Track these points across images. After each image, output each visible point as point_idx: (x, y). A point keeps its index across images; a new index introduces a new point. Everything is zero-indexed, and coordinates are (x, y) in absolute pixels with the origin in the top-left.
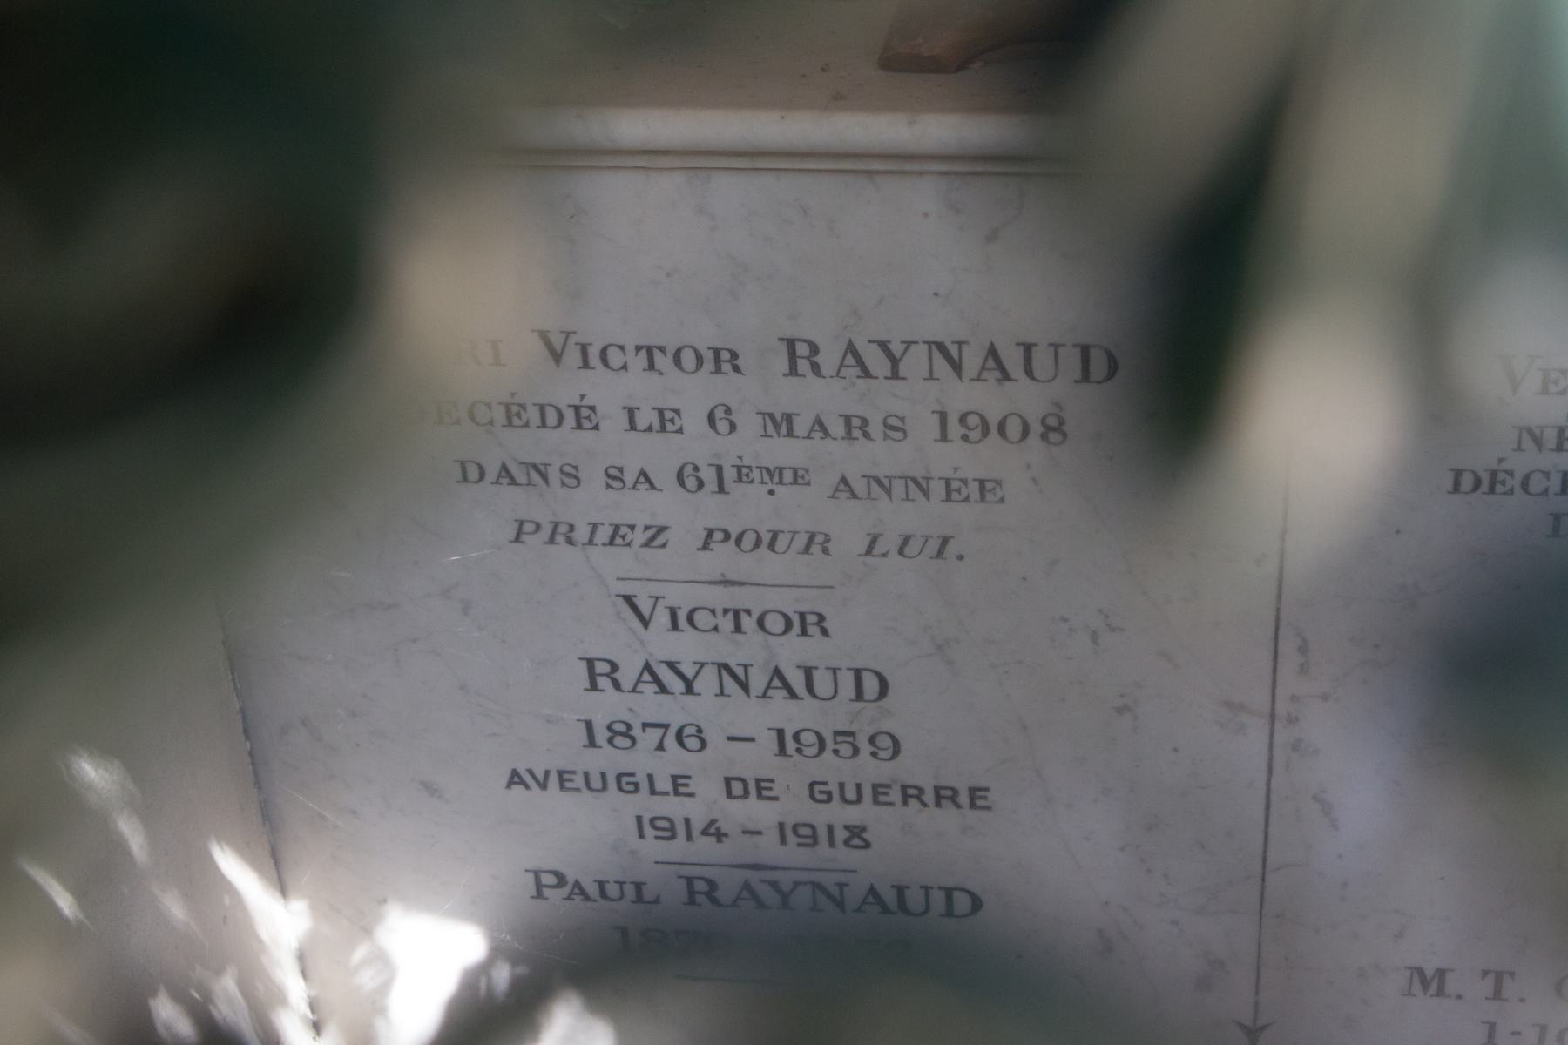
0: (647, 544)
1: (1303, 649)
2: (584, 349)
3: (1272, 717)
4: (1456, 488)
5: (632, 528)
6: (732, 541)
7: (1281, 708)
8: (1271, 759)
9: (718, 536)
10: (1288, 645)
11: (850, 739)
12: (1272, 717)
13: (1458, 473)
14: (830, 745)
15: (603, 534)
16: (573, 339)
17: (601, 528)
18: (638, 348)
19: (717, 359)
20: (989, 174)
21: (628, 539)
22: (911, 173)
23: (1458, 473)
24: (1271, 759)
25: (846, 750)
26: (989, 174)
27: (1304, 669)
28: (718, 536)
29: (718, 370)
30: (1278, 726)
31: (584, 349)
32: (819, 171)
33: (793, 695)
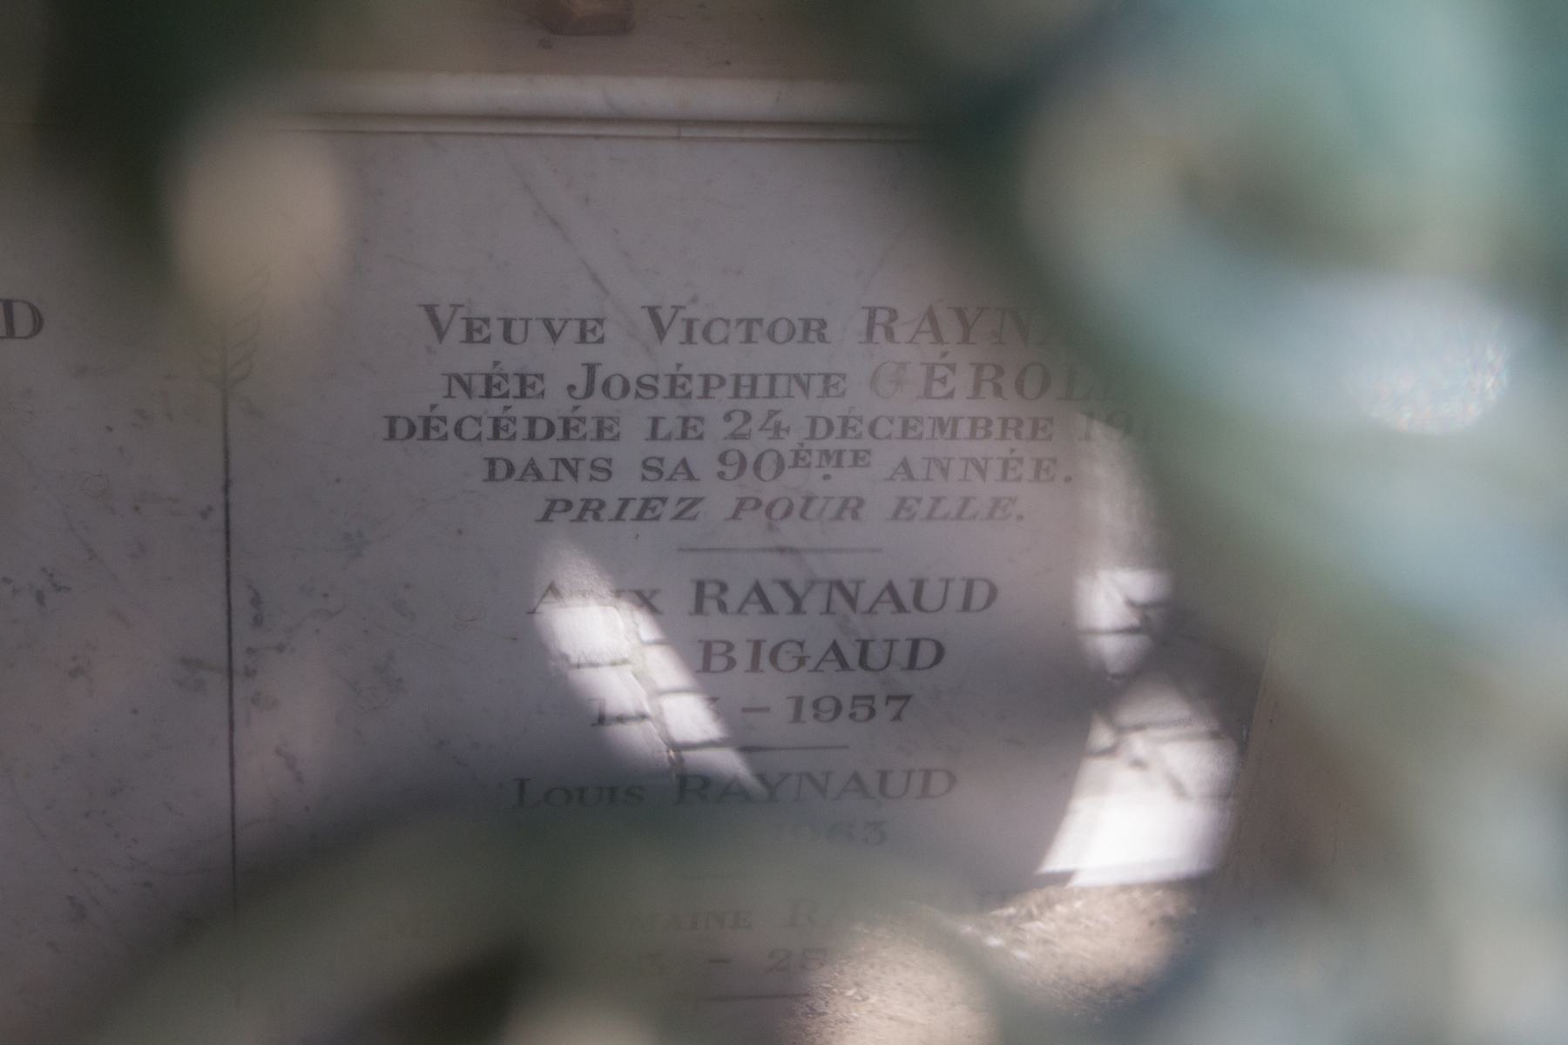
0: (678, 517)
1: (256, 601)
2: (690, 323)
3: (230, 672)
4: (392, 435)
5: (919, 500)
6: (762, 510)
7: (239, 661)
8: (231, 715)
9: (560, 506)
10: (241, 599)
11: (869, 702)
12: (230, 672)
13: (392, 420)
14: (847, 709)
15: (633, 509)
16: (682, 314)
17: (631, 504)
18: (740, 321)
19: (807, 329)
20: (792, 140)
21: (658, 512)
22: (603, 137)
23: (392, 420)
24: (231, 715)
25: (862, 712)
26: (792, 140)
27: (258, 621)
28: (560, 506)
29: (805, 339)
30: (237, 681)
31: (690, 323)
32: (635, 138)
33: (844, 665)
